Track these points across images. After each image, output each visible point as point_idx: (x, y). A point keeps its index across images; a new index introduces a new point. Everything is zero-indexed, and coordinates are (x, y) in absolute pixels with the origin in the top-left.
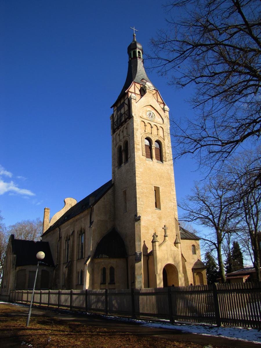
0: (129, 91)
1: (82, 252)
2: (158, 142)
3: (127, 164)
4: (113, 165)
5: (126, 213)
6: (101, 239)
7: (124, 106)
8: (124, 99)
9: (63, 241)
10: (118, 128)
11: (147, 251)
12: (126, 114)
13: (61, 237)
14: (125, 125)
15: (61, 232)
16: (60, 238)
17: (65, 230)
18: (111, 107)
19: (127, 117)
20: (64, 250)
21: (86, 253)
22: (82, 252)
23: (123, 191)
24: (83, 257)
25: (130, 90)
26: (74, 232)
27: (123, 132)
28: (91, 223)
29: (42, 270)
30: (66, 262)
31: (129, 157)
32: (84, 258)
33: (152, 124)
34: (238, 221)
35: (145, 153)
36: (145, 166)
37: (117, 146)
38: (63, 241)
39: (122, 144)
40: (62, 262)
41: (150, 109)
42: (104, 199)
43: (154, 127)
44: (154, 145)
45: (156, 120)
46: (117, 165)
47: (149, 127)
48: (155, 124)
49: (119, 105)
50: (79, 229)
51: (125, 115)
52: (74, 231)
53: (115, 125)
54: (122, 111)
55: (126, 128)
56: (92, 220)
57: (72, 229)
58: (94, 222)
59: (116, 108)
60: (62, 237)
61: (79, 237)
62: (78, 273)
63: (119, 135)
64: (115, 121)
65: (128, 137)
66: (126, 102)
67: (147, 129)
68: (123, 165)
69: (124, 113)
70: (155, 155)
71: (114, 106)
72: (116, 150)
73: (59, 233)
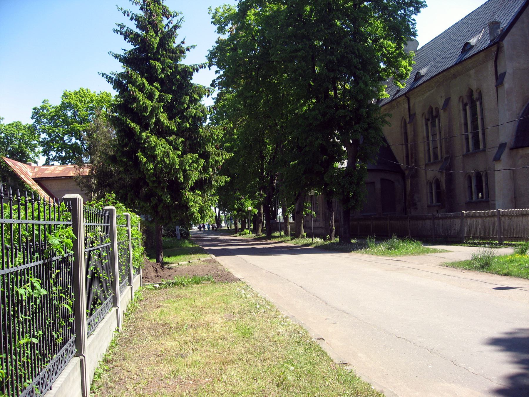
1: (475, 127)
6: (524, 108)
9: (421, 122)
13: (415, 114)
15: (411, 105)
16: (412, 116)
21: (489, 139)
22: (475, 127)
24: (481, 147)
26: (447, 101)
28: (500, 79)
30: (432, 161)
32: (484, 150)
34: (324, 303)
38: (421, 122)
50: (465, 93)
56: (500, 71)
57: (443, 95)
58: (507, 74)
60: (417, 113)
61: (465, 110)
62: (470, 178)
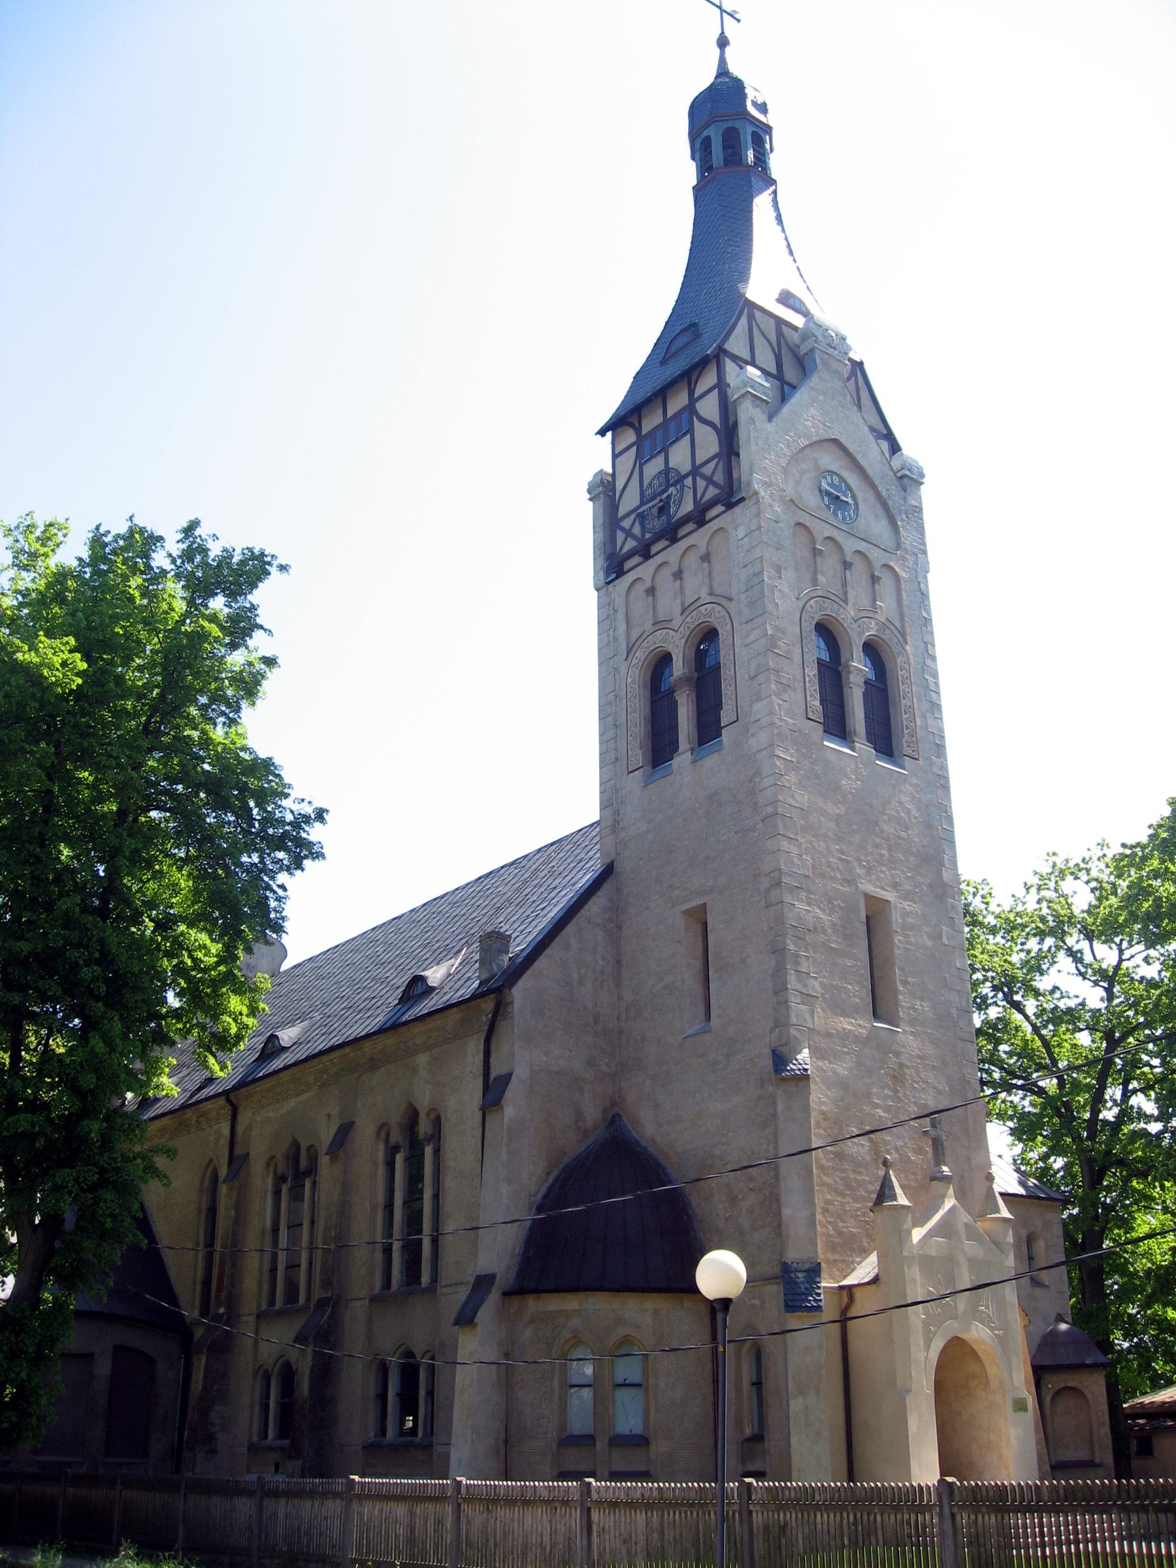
0: (725, 352)
2: (871, 649)
3: (711, 761)
4: (609, 759)
5: (707, 1038)
7: (691, 431)
8: (691, 392)
9: (260, 1181)
10: (645, 553)
11: (878, 1257)
12: (710, 481)
14: (700, 538)
15: (240, 1129)
17: (271, 1114)
18: (602, 433)
19: (712, 492)
20: (263, 1232)
23: (686, 913)
24: (425, 1279)
25: (727, 347)
26: (345, 1131)
27: (678, 575)
28: (494, 1090)
29: (115, 1346)
31: (724, 721)
32: (432, 1289)
33: (850, 545)
35: (817, 703)
36: (818, 777)
37: (640, 655)
38: (260, 1181)
39: (678, 647)
40: (249, 1305)
41: (829, 460)
42: (567, 948)
43: (859, 566)
44: (859, 667)
45: (861, 523)
46: (638, 757)
47: (829, 565)
48: (862, 546)
49: (650, 423)
50: (395, 1117)
51: (701, 484)
52: (352, 1124)
53: (629, 533)
54: (679, 456)
55: (706, 558)
57: (335, 1112)
58: (514, 1080)
59: (630, 437)
60: (254, 1153)
62: (383, 1368)
63: (651, 591)
64: (622, 511)
65: (718, 608)
66: (709, 407)
67: (822, 573)
68: (682, 760)
69: (695, 471)
70: (862, 715)
71: (614, 426)
72: (633, 676)
73: (226, 1131)
